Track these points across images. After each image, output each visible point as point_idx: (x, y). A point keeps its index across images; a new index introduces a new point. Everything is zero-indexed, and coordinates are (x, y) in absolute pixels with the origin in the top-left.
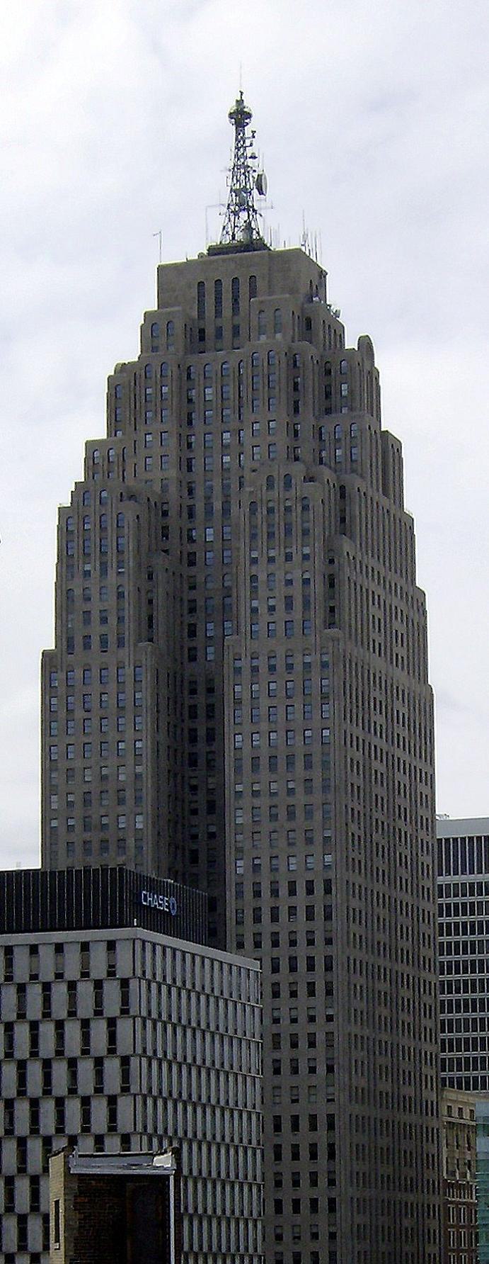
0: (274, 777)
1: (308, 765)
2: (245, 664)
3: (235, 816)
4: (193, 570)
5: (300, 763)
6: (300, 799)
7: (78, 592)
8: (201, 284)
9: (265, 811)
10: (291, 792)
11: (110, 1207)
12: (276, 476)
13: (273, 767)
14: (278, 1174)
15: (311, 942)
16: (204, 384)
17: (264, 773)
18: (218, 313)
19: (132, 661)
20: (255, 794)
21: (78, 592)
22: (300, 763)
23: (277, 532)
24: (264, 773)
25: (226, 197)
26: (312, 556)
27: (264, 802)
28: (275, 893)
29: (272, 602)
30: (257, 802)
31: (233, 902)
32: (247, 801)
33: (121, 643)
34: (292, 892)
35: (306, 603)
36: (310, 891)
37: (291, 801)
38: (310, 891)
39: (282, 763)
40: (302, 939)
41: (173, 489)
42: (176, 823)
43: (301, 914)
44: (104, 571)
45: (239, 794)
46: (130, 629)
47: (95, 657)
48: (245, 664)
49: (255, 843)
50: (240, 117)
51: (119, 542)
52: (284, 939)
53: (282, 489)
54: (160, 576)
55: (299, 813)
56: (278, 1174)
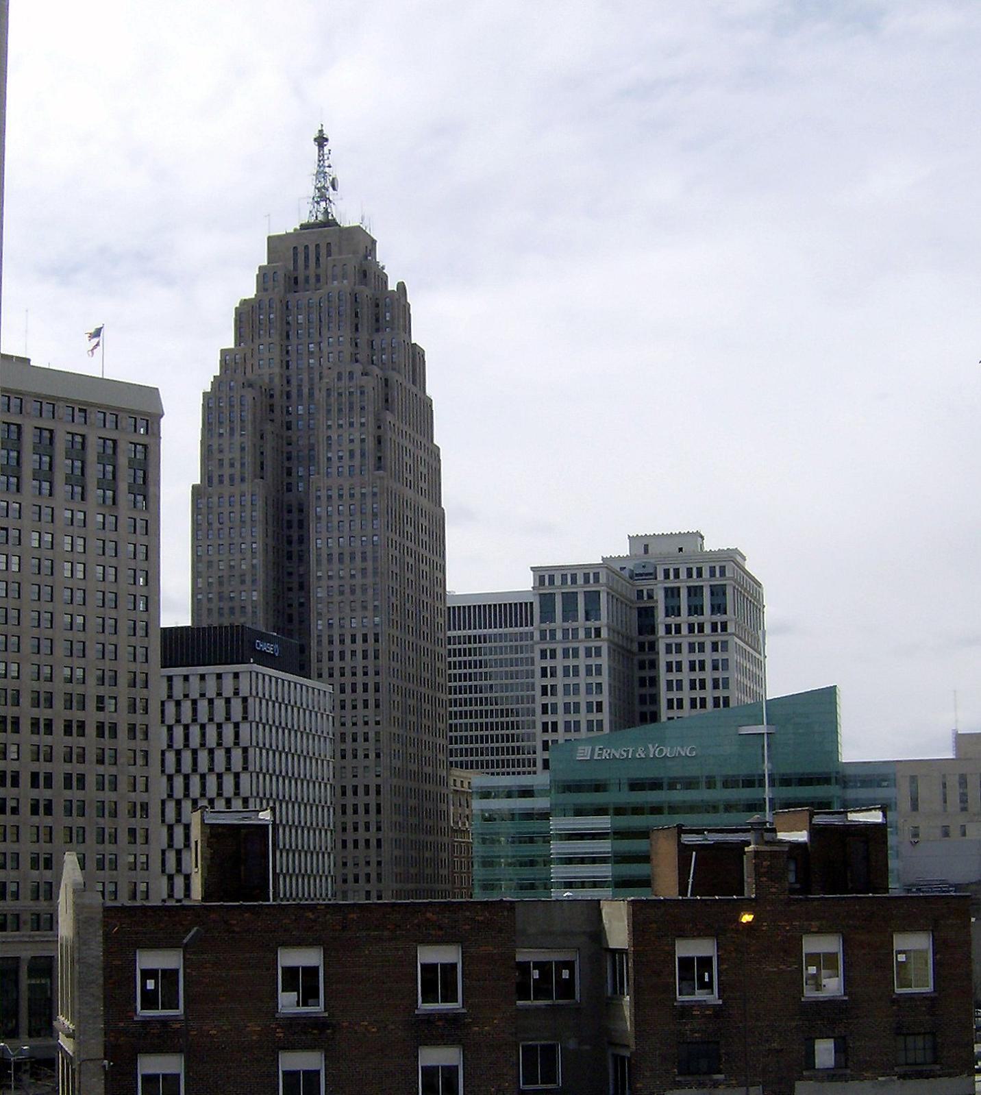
0: (342, 567)
6: (359, 581)
13: (341, 560)
15: (365, 674)
18: (307, 266)
21: (215, 447)
24: (336, 565)
27: (335, 583)
28: (342, 642)
29: (340, 454)
33: (243, 480)
37: (353, 582)
39: (347, 558)
48: (323, 493)
50: (321, 141)
55: (358, 591)
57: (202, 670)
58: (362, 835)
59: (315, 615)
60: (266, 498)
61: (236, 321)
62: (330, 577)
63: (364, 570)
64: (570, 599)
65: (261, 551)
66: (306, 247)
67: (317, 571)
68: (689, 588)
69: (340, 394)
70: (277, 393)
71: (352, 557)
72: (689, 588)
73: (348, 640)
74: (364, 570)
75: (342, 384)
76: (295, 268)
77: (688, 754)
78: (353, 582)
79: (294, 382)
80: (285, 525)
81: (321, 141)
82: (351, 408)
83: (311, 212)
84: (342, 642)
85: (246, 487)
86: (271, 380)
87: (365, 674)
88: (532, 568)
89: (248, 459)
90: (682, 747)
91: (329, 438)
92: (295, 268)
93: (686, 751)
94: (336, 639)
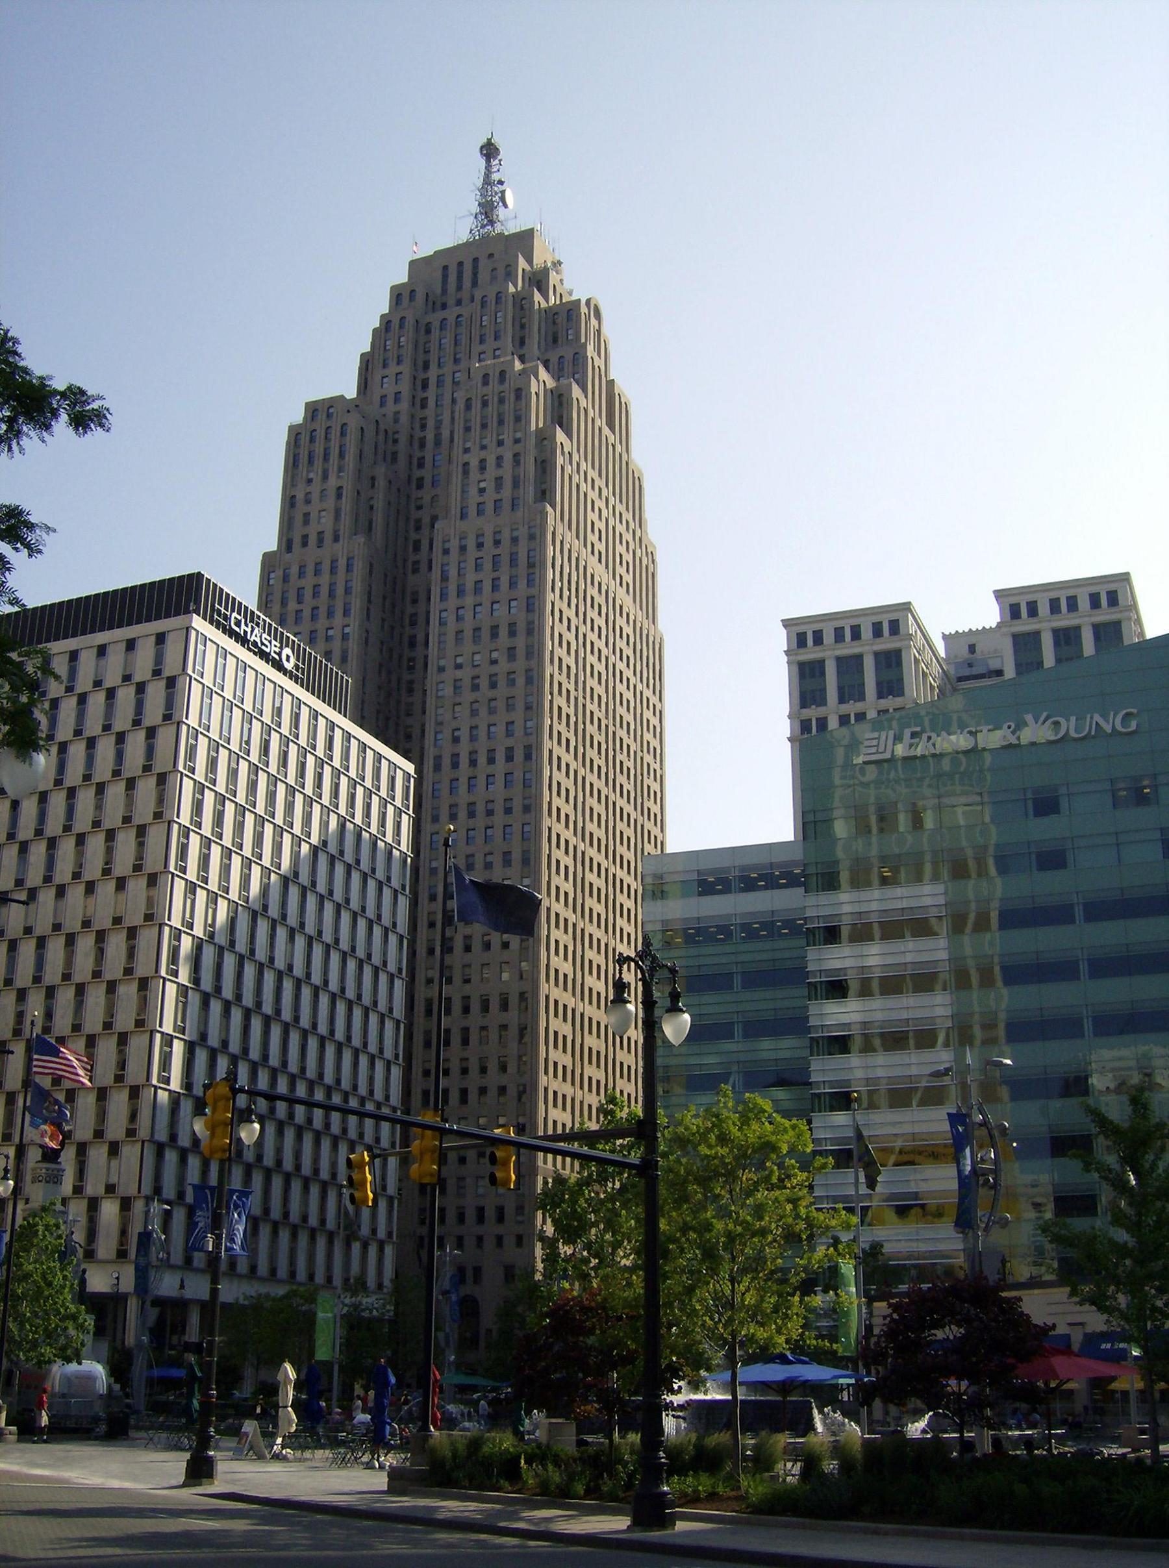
0: (476, 648)
1: (512, 633)
2: (454, 544)
3: (438, 690)
4: (420, 493)
5: (503, 632)
6: (504, 666)
7: (300, 496)
8: (445, 268)
9: (467, 683)
10: (494, 662)
11: (681, 1310)
12: (491, 374)
13: (476, 639)
14: (464, 1059)
15: (508, 811)
16: (480, 435)
17: (468, 647)
18: (459, 288)
19: (345, 554)
20: (459, 667)
21: (300, 496)
22: (503, 632)
23: (489, 424)
24: (468, 647)
25: (475, 208)
26: (523, 440)
27: (465, 675)
28: (473, 763)
29: (482, 485)
30: (459, 674)
31: (431, 774)
32: (450, 674)
33: (336, 539)
34: (491, 761)
35: (516, 484)
36: (509, 758)
37: (494, 669)
38: (509, 758)
39: (485, 634)
40: (499, 807)
41: (404, 419)
42: (388, 719)
43: (500, 780)
44: (325, 477)
45: (441, 669)
46: (346, 520)
47: (312, 554)
48: (454, 544)
49: (456, 715)
50: (489, 151)
51: (527, 777)
52: (480, 808)
53: (496, 382)
54: (381, 483)
55: (502, 682)
56: (464, 1059)
57: (101, 638)
58: (494, 1078)
59: (433, 724)
60: (371, 565)
61: (360, 369)
62: (459, 667)
63: (511, 650)
64: (850, 666)
65: (356, 636)
66: (460, 264)
67: (439, 659)
68: (1056, 632)
69: (485, 404)
70: (403, 439)
71: (494, 632)
72: (1056, 632)
73: (482, 759)
74: (511, 650)
75: (488, 390)
76: (444, 291)
77: (1119, 727)
78: (494, 669)
79: (431, 424)
80: (407, 621)
81: (489, 151)
82: (501, 422)
83: (471, 230)
84: (473, 763)
85: (341, 550)
86: (396, 421)
87: (508, 811)
88: (782, 621)
89: (346, 504)
90: (1105, 716)
91: (466, 464)
92: (444, 291)
93: (1112, 722)
94: (464, 760)
